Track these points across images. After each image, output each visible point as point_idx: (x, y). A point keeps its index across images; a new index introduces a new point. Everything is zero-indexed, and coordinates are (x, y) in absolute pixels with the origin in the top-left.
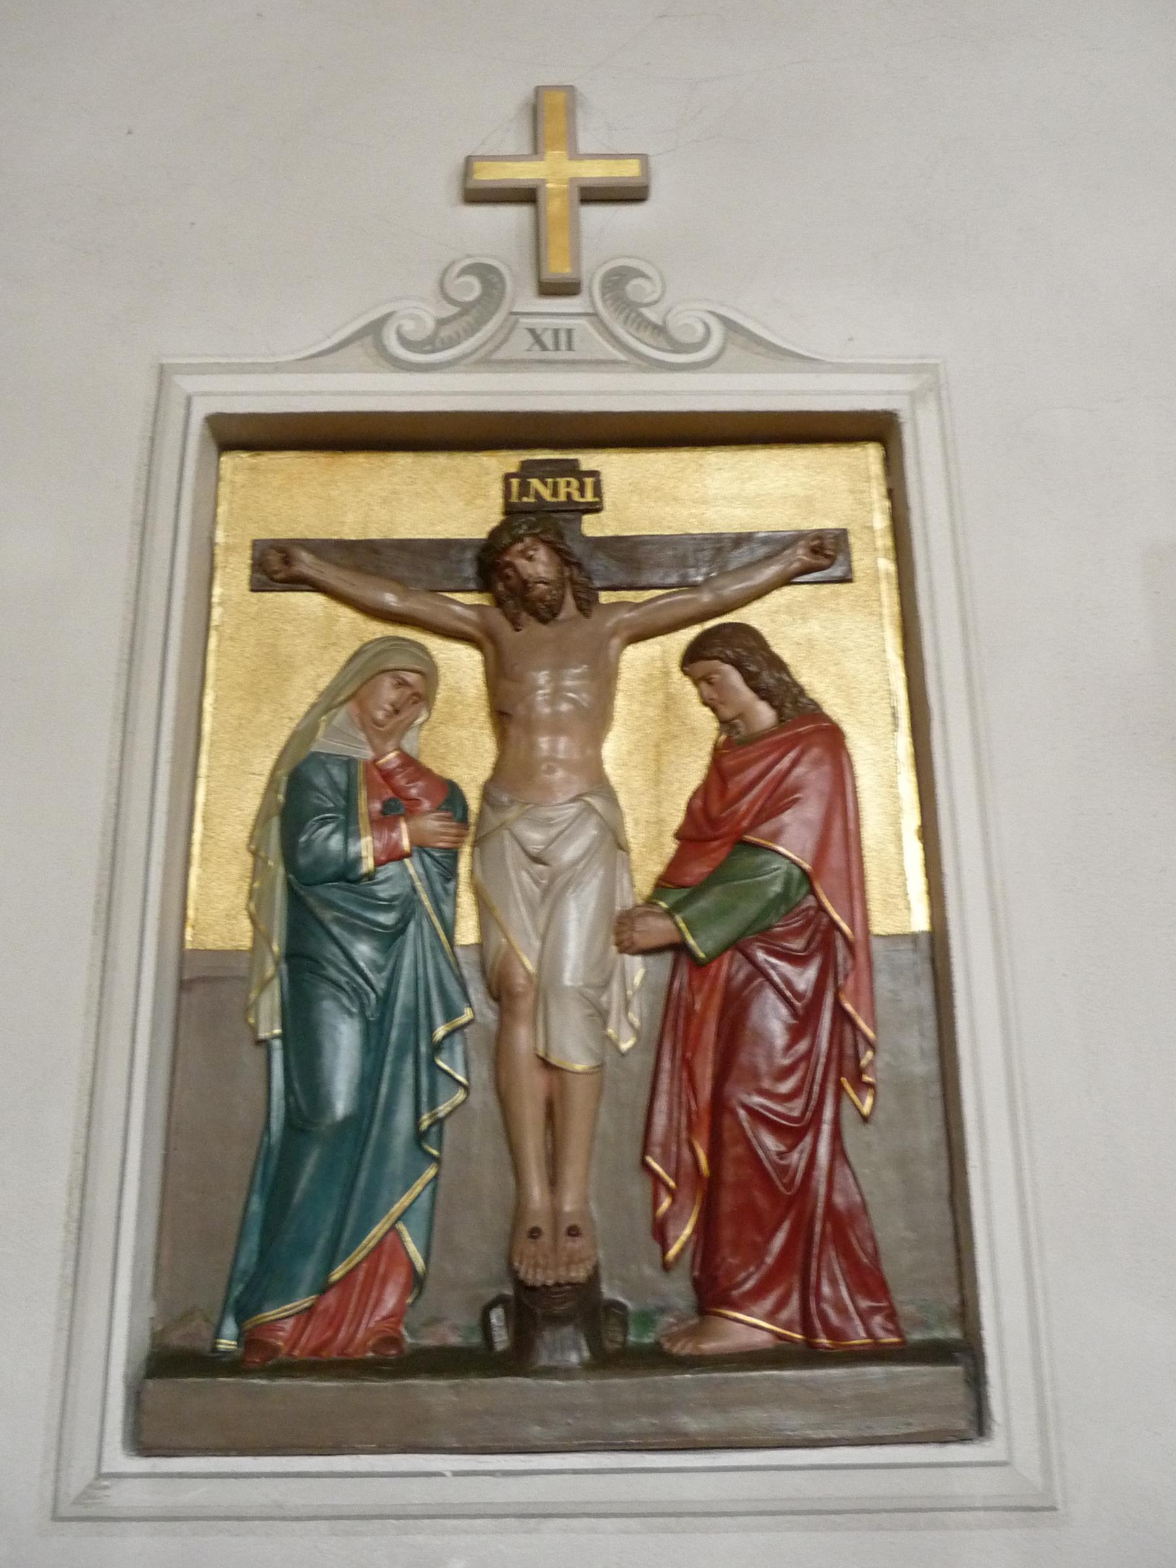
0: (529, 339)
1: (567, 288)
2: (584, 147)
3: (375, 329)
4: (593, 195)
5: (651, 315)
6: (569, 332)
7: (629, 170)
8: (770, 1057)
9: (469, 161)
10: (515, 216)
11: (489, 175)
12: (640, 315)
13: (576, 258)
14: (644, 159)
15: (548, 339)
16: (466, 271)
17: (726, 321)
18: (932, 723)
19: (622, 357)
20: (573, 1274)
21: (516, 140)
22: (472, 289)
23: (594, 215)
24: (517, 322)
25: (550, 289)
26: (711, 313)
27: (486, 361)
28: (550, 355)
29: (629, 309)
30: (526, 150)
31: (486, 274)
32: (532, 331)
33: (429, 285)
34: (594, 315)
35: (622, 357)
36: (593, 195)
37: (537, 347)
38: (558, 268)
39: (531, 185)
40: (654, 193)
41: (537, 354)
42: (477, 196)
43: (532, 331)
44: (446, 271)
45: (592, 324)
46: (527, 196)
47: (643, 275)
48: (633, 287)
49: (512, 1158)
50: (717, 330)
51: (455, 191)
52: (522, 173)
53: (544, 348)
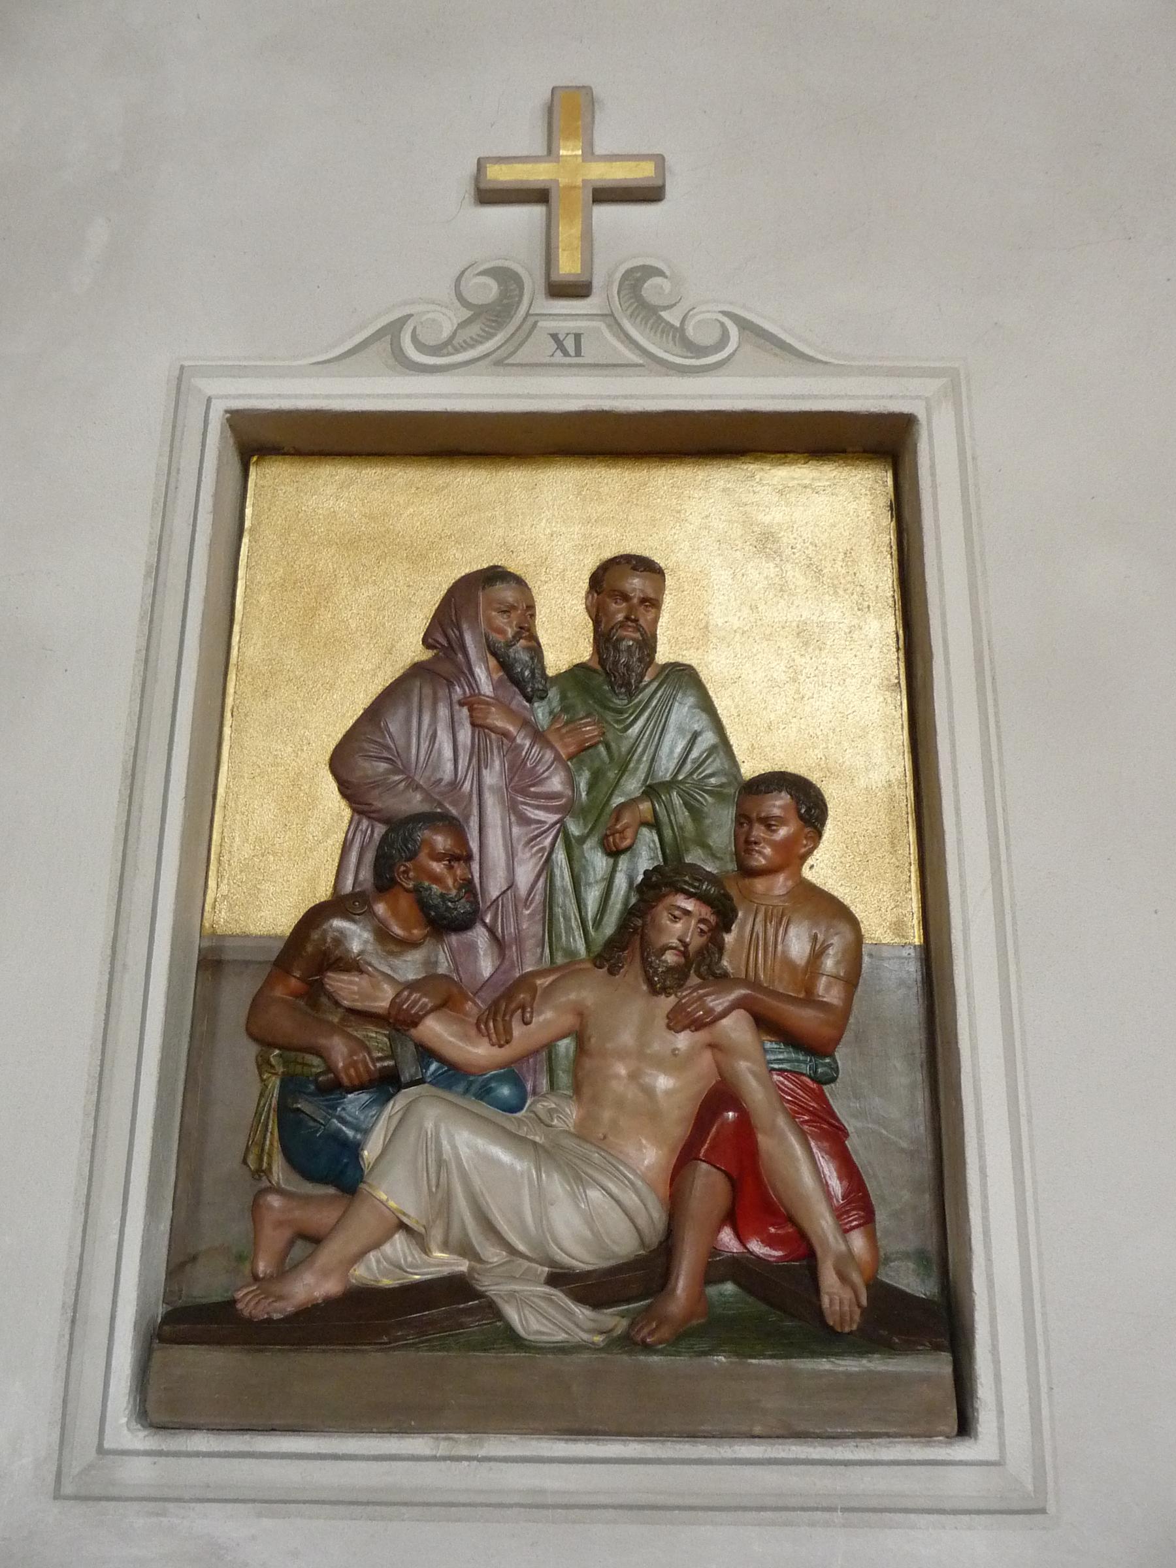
0: (553, 345)
1: (578, 290)
2: (602, 146)
3: (393, 330)
4: (605, 195)
5: (672, 317)
6: (578, 337)
7: (642, 173)
8: (838, 1201)
9: (481, 164)
10: (531, 215)
11: (500, 175)
12: (660, 317)
13: (588, 261)
14: (660, 161)
15: (570, 344)
16: (485, 273)
17: (744, 325)
18: (594, 409)
19: (634, 358)
20: (528, 954)
21: (529, 139)
22: (490, 290)
23: (604, 213)
24: (536, 323)
25: (560, 290)
26: (724, 313)
27: (501, 363)
28: (567, 360)
29: (647, 312)
30: (541, 150)
31: (506, 277)
32: (554, 336)
33: (445, 292)
34: (609, 317)
35: (634, 358)
36: (605, 195)
37: (559, 353)
38: (568, 266)
39: (542, 186)
40: (672, 190)
41: (559, 357)
42: (489, 196)
43: (554, 336)
44: (458, 280)
45: (609, 326)
46: (540, 196)
47: (660, 273)
48: (651, 289)
49: (446, 455)
50: (733, 331)
51: (468, 188)
52: (538, 174)
53: (566, 353)
